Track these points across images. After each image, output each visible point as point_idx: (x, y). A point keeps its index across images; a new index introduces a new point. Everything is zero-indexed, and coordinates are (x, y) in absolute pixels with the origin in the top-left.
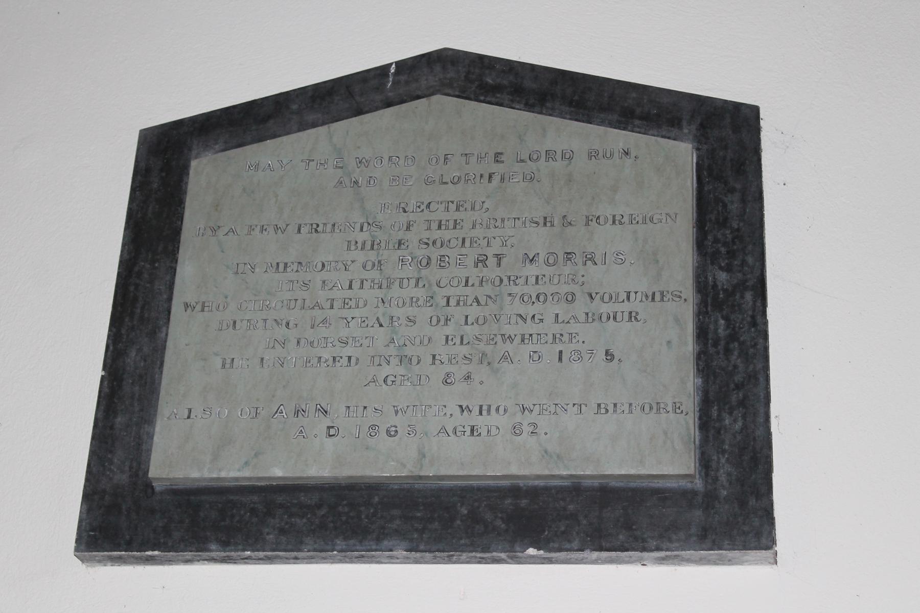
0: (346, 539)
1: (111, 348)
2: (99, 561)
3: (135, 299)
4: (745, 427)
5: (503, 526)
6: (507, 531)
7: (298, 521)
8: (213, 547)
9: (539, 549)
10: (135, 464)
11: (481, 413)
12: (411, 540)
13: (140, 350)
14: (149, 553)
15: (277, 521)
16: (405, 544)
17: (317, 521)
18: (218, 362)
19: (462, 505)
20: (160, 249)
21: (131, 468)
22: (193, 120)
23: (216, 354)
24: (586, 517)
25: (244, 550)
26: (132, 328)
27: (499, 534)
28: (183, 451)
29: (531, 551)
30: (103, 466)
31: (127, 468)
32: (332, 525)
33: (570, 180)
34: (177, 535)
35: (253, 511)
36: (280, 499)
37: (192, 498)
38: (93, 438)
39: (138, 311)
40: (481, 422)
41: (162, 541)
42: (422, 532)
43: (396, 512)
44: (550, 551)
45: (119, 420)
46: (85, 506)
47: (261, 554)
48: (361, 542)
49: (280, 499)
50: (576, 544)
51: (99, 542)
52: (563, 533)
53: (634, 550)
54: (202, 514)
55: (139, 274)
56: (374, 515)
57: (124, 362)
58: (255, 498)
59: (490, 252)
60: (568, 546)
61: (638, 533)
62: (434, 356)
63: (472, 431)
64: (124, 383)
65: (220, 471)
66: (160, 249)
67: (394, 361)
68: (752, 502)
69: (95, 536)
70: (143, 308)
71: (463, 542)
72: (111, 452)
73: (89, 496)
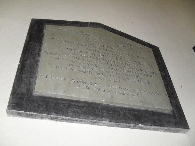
0: (92, 116)
1: (22, 58)
2: (13, 114)
3: (29, 49)
4: (176, 102)
5: (132, 118)
6: (133, 119)
7: (78, 110)
8: (53, 114)
9: (142, 124)
10: (28, 88)
11: (124, 90)
12: (110, 119)
13: (31, 60)
14: (32, 113)
15: (72, 109)
16: (108, 120)
17: (84, 111)
18: (55, 66)
19: (121, 111)
20: (37, 41)
21: (27, 89)
22: (45, 20)
23: (54, 64)
24: (150, 118)
25: (63, 116)
26: (28, 55)
27: (132, 120)
28: (44, 86)
29: (140, 125)
30: (18, 87)
31: (26, 88)
32: (88, 112)
33: (131, 49)
34: (42, 109)
35: (65, 105)
36: (72, 103)
37: (46, 99)
38: (15, 79)
39: (30, 52)
40: (124, 91)
41: (37, 110)
42: (113, 117)
43: (105, 111)
44: (145, 125)
45: (24, 76)
46: (12, 97)
47: (67, 118)
48: (96, 118)
49: (72, 103)
50: (150, 124)
51: (16, 107)
52: (146, 121)
53: (162, 126)
54: (49, 104)
55: (31, 45)
56: (99, 111)
57: (26, 62)
58: (65, 102)
59: (119, 57)
60: (148, 124)
61: (162, 123)
62: (110, 75)
63: (123, 93)
64: (26, 67)
65: (57, 92)
66: (37, 41)
67: (101, 75)
68: (182, 118)
69: (14, 106)
70: (31, 52)
71: (123, 121)
72: (21, 83)
73: (13, 94)
